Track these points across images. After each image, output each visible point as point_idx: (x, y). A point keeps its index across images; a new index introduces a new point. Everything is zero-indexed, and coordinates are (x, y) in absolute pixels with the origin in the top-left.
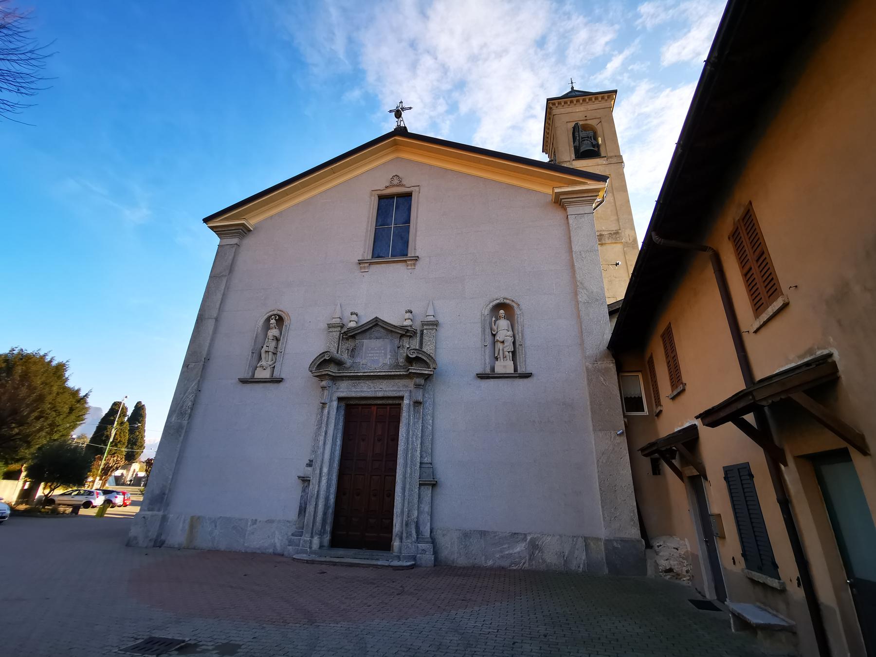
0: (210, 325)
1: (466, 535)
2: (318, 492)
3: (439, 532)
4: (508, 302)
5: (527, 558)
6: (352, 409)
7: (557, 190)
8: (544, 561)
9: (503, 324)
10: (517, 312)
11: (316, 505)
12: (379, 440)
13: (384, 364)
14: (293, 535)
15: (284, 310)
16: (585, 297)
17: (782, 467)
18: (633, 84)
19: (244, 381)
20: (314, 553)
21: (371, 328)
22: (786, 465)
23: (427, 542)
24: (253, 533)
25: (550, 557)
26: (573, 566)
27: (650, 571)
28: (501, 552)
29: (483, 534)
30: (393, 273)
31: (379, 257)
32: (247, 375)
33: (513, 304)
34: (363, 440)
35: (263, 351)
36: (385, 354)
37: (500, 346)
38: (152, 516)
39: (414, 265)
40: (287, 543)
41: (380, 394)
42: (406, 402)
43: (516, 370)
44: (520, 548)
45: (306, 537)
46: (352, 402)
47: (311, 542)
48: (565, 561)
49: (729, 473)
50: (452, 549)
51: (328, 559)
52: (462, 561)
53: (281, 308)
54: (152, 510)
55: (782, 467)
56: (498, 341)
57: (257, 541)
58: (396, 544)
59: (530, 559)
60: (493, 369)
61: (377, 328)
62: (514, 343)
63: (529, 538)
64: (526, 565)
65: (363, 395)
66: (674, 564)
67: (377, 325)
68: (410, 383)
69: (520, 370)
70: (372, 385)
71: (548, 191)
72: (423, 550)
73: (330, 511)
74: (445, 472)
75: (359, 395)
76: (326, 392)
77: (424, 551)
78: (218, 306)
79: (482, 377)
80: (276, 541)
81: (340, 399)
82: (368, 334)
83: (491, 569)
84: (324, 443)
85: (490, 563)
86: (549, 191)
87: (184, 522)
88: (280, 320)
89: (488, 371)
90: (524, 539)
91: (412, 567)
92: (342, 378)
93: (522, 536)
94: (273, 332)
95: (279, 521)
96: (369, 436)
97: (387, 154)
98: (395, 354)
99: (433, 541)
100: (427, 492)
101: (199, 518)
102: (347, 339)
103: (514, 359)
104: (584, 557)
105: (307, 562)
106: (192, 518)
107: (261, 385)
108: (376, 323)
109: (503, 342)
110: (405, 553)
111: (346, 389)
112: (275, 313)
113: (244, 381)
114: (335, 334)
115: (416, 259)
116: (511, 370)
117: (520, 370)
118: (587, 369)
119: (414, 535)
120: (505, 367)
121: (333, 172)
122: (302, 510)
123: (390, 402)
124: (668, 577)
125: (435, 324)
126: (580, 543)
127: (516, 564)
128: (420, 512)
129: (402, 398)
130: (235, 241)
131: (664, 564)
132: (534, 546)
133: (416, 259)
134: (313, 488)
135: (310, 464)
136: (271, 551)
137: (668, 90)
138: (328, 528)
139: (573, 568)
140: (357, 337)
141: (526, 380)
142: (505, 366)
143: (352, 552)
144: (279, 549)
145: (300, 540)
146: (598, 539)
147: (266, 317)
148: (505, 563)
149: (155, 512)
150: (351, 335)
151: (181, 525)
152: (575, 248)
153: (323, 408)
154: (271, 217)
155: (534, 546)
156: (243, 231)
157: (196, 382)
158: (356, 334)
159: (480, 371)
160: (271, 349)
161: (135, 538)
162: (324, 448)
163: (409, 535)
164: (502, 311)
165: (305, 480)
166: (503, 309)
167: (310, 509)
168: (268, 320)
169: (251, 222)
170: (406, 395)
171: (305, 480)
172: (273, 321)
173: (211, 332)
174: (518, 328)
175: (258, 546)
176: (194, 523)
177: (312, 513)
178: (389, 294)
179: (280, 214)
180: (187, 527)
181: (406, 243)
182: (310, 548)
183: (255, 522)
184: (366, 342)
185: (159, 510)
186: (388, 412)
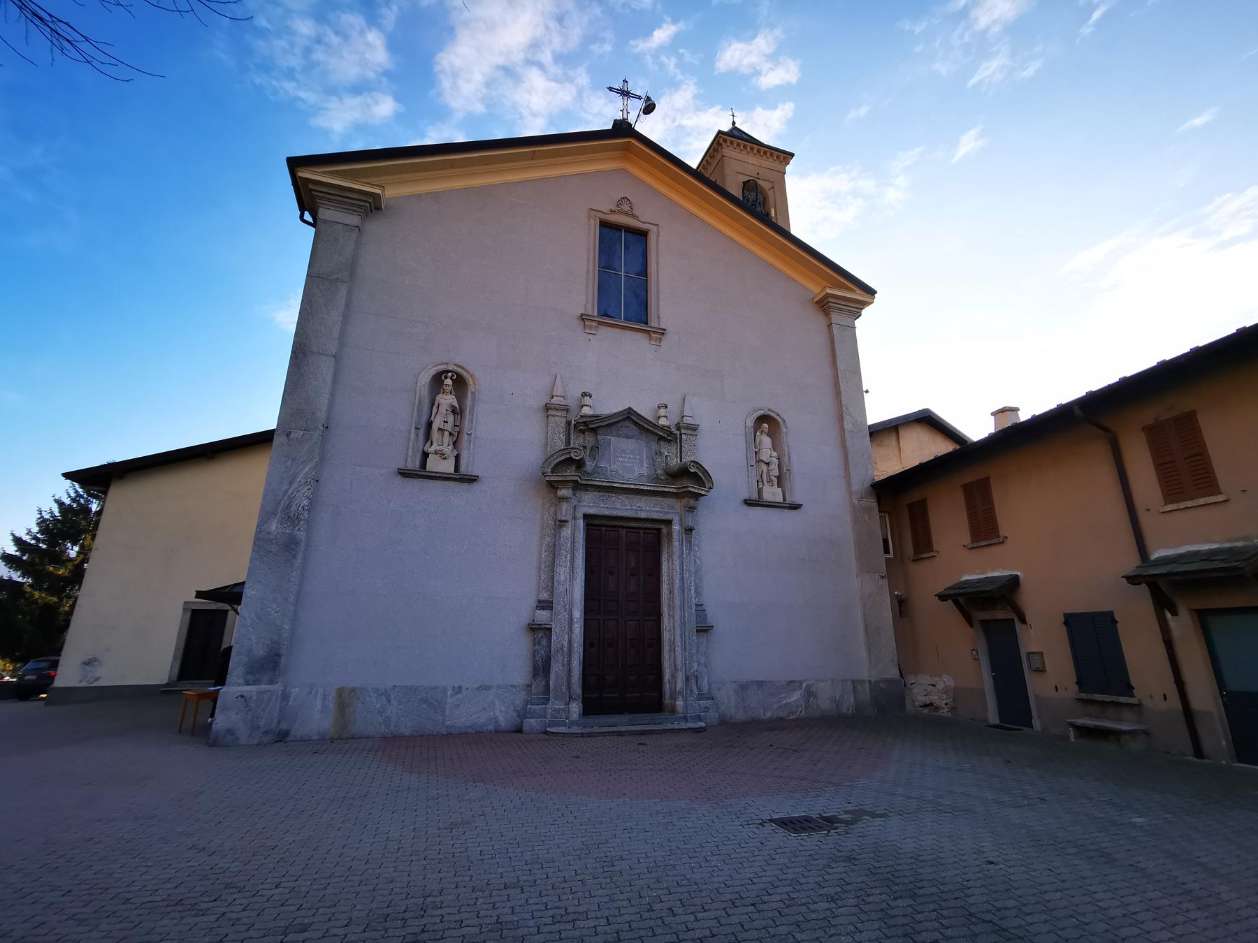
0: (325, 368)
1: (743, 687)
2: (570, 642)
3: (714, 685)
6: (600, 532)
7: (829, 291)
9: (767, 441)
12: (633, 575)
13: (641, 475)
14: (528, 702)
17: (1169, 615)
18: (680, 77)
19: (405, 474)
22: (1174, 613)
24: (458, 706)
26: (844, 710)
27: (909, 707)
29: (760, 684)
30: (623, 347)
31: (606, 315)
32: (414, 464)
34: (611, 574)
36: (641, 461)
38: (259, 693)
39: (660, 340)
41: (643, 515)
42: (676, 527)
44: (796, 696)
46: (597, 522)
49: (197, 597)
52: (740, 716)
54: (255, 683)
55: (1169, 615)
57: (465, 715)
61: (627, 423)
65: (614, 513)
66: (935, 698)
67: (628, 418)
68: (678, 505)
71: (816, 289)
76: (565, 506)
79: (749, 503)
80: (498, 713)
81: (586, 516)
83: (770, 720)
85: (769, 715)
86: (816, 290)
87: (325, 697)
88: (460, 383)
89: (755, 496)
92: (586, 488)
94: (447, 400)
95: (499, 687)
96: (625, 567)
97: (612, 159)
98: (653, 463)
101: (353, 690)
102: (583, 432)
106: (340, 691)
107: (439, 483)
108: (629, 416)
109: (768, 464)
111: (591, 504)
112: (451, 367)
113: (405, 474)
114: (559, 419)
115: (662, 332)
117: (463, 469)
118: (854, 506)
120: (774, 494)
121: (533, 156)
122: (541, 668)
124: (926, 711)
125: (694, 428)
129: (669, 523)
130: (353, 219)
131: (922, 699)
132: (810, 694)
133: (662, 332)
134: (559, 638)
136: (491, 727)
137: (718, 107)
138: (577, 689)
140: (600, 431)
141: (794, 512)
142: (772, 493)
143: (625, 718)
144: (503, 723)
146: (863, 681)
147: (434, 371)
148: (783, 714)
149: (263, 687)
151: (319, 703)
152: (840, 366)
153: (560, 527)
154: (419, 196)
155: (810, 694)
156: (371, 206)
159: (746, 496)
161: (230, 732)
164: (766, 425)
165: (533, 628)
166: (767, 422)
167: (557, 668)
168: (438, 380)
169: (391, 192)
170: (676, 519)
172: (449, 382)
173: (329, 378)
176: (345, 700)
178: (620, 373)
179: (435, 195)
181: (645, 305)
183: (459, 690)
185: (271, 682)
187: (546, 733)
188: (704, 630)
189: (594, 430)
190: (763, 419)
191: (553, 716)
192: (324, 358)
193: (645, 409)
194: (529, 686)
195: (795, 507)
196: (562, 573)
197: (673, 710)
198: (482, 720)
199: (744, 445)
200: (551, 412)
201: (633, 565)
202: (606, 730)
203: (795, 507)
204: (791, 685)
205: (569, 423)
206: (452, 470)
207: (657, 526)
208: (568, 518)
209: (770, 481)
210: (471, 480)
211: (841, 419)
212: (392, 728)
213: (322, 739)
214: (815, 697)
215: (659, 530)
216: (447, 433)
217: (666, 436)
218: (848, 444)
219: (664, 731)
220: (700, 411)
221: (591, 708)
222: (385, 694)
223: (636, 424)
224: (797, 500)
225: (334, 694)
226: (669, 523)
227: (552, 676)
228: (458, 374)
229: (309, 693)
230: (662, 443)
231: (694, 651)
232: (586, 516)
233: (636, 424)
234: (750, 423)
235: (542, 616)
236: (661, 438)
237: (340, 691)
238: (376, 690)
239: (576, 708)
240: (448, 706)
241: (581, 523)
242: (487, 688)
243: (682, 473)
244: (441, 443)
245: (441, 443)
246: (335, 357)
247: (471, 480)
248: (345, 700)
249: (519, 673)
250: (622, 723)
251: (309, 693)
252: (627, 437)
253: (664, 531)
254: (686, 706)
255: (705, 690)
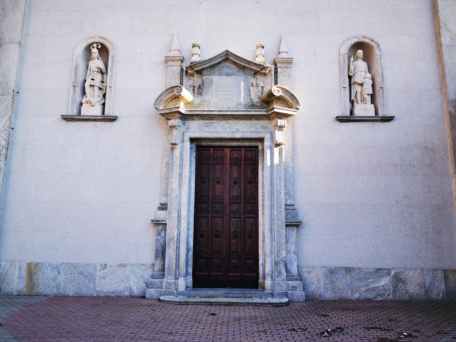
1: (332, 272)
3: (304, 269)
4: (367, 41)
5: (392, 290)
6: (204, 151)
8: (407, 292)
9: (361, 65)
10: (377, 52)
11: (178, 248)
12: (235, 183)
13: (240, 104)
14: (153, 277)
15: (107, 38)
16: (449, 40)
19: (67, 119)
20: (182, 294)
21: (219, 63)
23: (297, 280)
25: (413, 287)
26: (434, 295)
28: (367, 286)
29: (348, 270)
32: (73, 112)
33: (372, 43)
34: (218, 183)
35: (87, 85)
37: (358, 88)
40: (144, 285)
41: (238, 136)
43: (376, 113)
44: (384, 282)
45: (169, 279)
46: (204, 144)
47: (176, 285)
48: (426, 291)
50: (319, 285)
51: (197, 299)
52: (329, 295)
53: (103, 34)
56: (356, 83)
58: (268, 283)
59: (394, 291)
60: (352, 112)
61: (227, 64)
62: (373, 86)
63: (393, 273)
64: (391, 296)
67: (227, 60)
69: (381, 114)
70: (227, 126)
72: (293, 287)
73: (191, 253)
74: (305, 213)
75: (214, 135)
76: (175, 132)
77: (294, 288)
78: (19, 28)
80: (132, 284)
81: (192, 140)
82: (216, 69)
83: (358, 301)
84: (180, 186)
85: (356, 296)
87: (20, 269)
88: (104, 50)
90: (389, 274)
91: (287, 304)
93: (387, 271)
95: (133, 265)
96: (226, 177)
99: (300, 277)
100: (293, 232)
102: (192, 75)
103: (373, 101)
104: (443, 287)
105: (180, 303)
106: (29, 265)
108: (227, 57)
109: (362, 85)
110: (277, 290)
111: (198, 129)
112: (97, 40)
113: (67, 119)
114: (175, 68)
116: (372, 113)
117: (381, 114)
118: (450, 113)
119: (284, 273)
120: (366, 110)
122: (161, 253)
123: (247, 144)
125: (289, 62)
126: (440, 274)
127: (381, 296)
128: (288, 252)
129: (261, 140)
132: (398, 279)
134: (172, 231)
135: (163, 207)
136: (127, 294)
138: (190, 270)
139: (434, 297)
140: (205, 72)
141: (386, 124)
142: (364, 109)
143: (221, 291)
144: (136, 292)
145: (161, 282)
150: (196, 71)
151: (17, 272)
153: (173, 149)
155: (398, 279)
157: (7, 117)
158: (203, 69)
160: (97, 83)
162: (180, 192)
163: (280, 273)
166: (362, 49)
167: (170, 252)
168: (88, 49)
171: (159, 225)
172: (95, 51)
174: (377, 68)
175: (111, 290)
177: (174, 257)
180: (24, 273)
182: (176, 289)
183: (105, 266)
184: (215, 78)
186: (248, 155)
187: (160, 300)
188: (294, 224)
189: (199, 72)
190: (358, 46)
191: (166, 288)
192: (12, 45)
193: (243, 51)
194: (154, 265)
195: (388, 119)
196: (175, 182)
197: (264, 288)
198: (121, 288)
199: (337, 70)
200: (169, 63)
201: (236, 175)
202: (204, 300)
203: (388, 119)
204: (379, 272)
205: (182, 70)
206: (373, 115)
207: (254, 144)
208: (177, 142)
209: (363, 100)
210: (113, 119)
211: (437, 35)
212: (61, 290)
213: (25, 295)
214: (404, 283)
215: (257, 147)
216: (96, 88)
217: (258, 71)
218: (446, 57)
219: (248, 304)
220: (292, 47)
221: (199, 281)
222: (56, 268)
223: (234, 63)
224: (389, 114)
225: (25, 267)
226: (261, 140)
227: (167, 258)
228: (102, 44)
229: (11, 265)
230: (258, 77)
231: (283, 241)
232: (192, 140)
233: (234, 63)
234: (345, 50)
235: (162, 215)
236: (256, 73)
237: (29, 265)
238: (51, 265)
239: (183, 283)
240: (97, 277)
241: (188, 144)
242: (124, 266)
243: (269, 99)
244: (93, 96)
245: (93, 96)
246: (20, 44)
247: (113, 119)
248: (32, 271)
249: (148, 256)
250: (220, 295)
251: (11, 265)
252: (227, 75)
253: (260, 147)
254: (273, 286)
255: (295, 271)
